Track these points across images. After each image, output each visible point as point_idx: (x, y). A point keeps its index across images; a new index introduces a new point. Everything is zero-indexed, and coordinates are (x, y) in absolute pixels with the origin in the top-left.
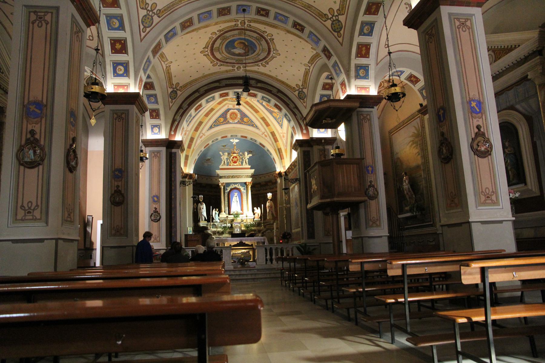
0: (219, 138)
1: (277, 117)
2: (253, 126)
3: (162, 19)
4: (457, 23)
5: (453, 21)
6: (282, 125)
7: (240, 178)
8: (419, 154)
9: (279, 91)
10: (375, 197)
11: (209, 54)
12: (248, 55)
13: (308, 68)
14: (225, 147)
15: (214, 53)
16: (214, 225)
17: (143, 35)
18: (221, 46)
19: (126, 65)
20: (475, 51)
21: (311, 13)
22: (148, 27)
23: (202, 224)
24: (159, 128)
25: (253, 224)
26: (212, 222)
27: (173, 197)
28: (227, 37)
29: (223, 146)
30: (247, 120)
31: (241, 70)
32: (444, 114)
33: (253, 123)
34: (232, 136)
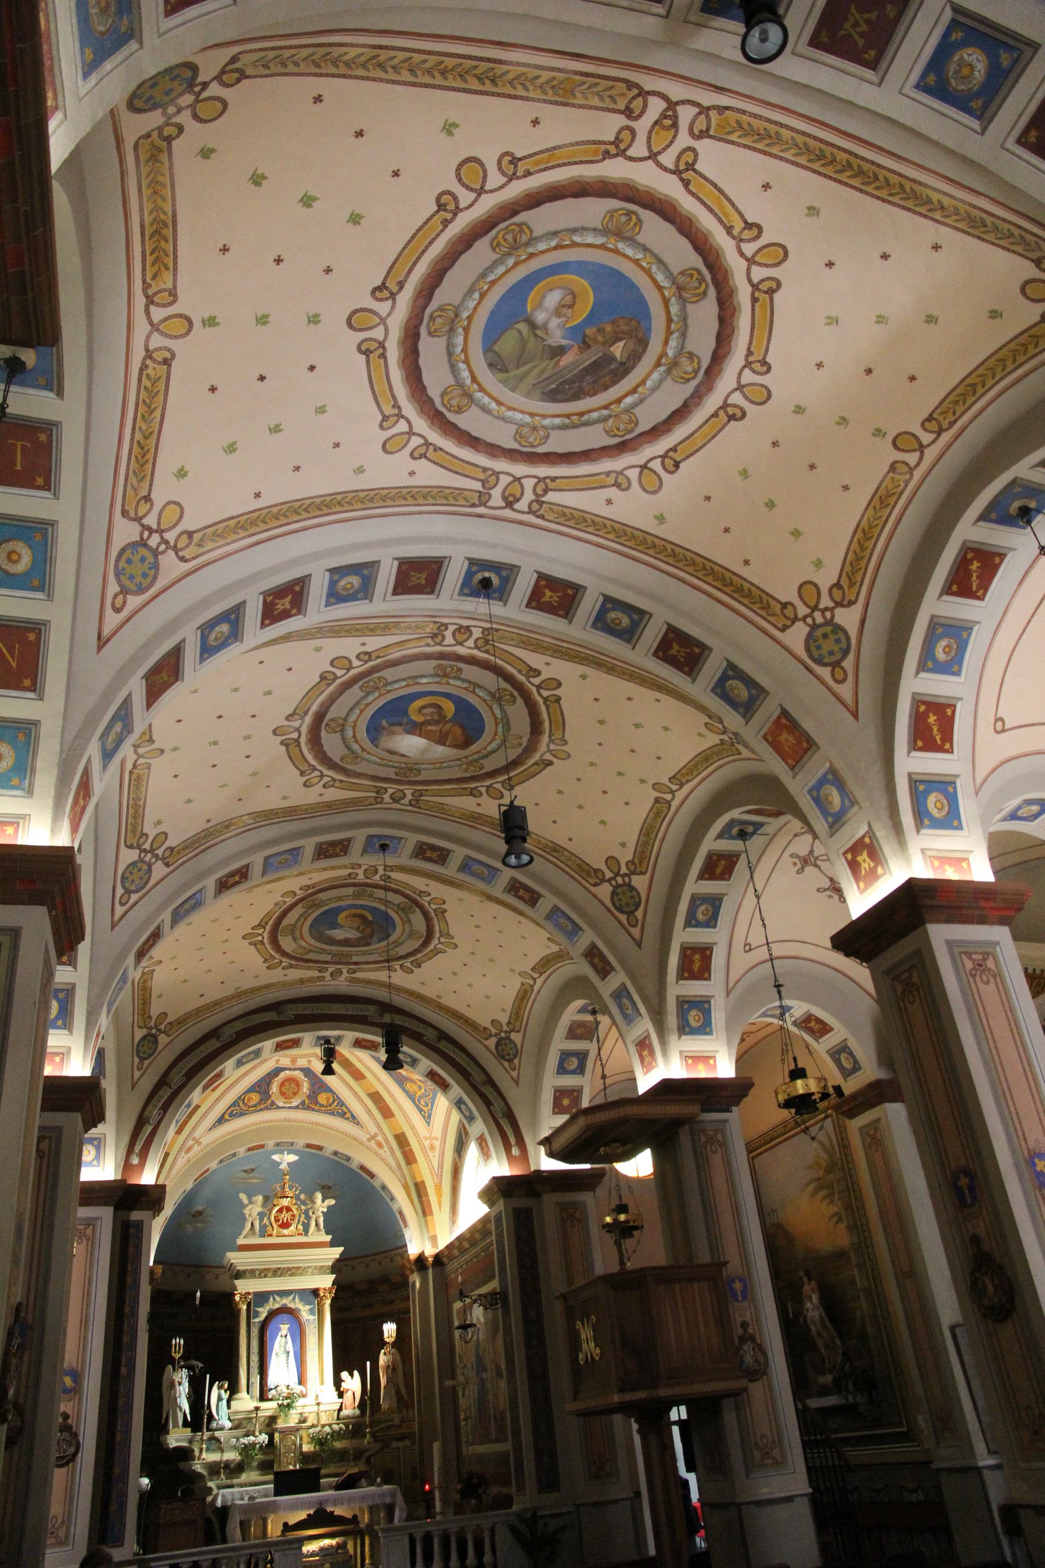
0: (242, 1151)
1: (419, 1094)
2: (343, 1115)
3: (173, 871)
4: (969, 965)
5: (958, 957)
6: (429, 1117)
7: (301, 1275)
8: (840, 1220)
9: (443, 1036)
10: (759, 1371)
11: (266, 941)
12: (369, 944)
13: (531, 982)
14: (252, 1175)
15: (280, 938)
16: (213, 1438)
17: (119, 910)
18: (300, 923)
19: (67, 994)
20: (1017, 1029)
21: (559, 863)
22: (637, 908)
23: (176, 1438)
24: (98, 1148)
25: (341, 1429)
26: (208, 1430)
27: (124, 1370)
28: (324, 901)
29: (245, 1171)
30: (328, 1099)
31: (342, 978)
32: (972, 1189)
33: (344, 1108)
34: (278, 1144)
